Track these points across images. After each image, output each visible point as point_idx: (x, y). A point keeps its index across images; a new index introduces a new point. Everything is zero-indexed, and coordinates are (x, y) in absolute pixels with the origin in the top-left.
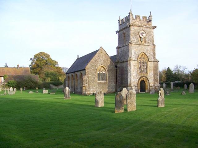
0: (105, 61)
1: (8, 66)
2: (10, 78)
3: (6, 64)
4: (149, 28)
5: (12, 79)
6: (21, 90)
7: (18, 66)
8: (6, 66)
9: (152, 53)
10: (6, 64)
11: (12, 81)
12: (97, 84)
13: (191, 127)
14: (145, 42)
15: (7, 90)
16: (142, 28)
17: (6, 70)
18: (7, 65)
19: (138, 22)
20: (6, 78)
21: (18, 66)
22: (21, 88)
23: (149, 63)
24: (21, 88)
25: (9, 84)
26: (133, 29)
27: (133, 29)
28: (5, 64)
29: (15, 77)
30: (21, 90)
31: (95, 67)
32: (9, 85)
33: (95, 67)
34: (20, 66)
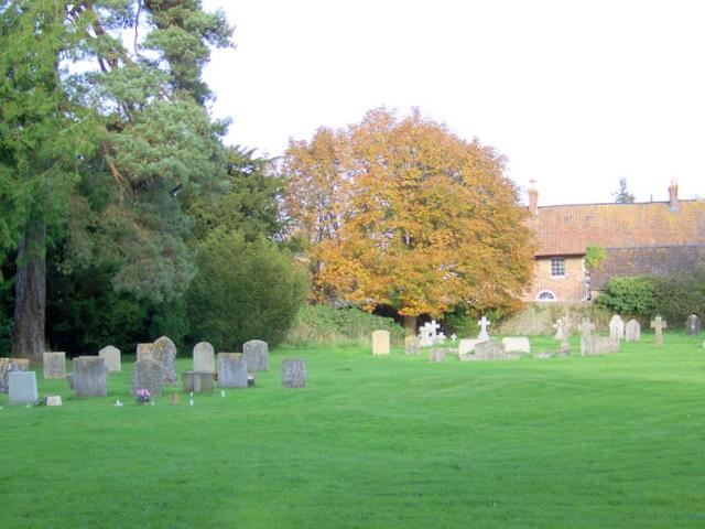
1: (632, 198)
2: (620, 262)
3: (623, 183)
4: (651, 503)
5: (629, 271)
6: (484, 328)
7: (673, 191)
8: (625, 199)
10: (623, 183)
11: (623, 282)
12: (140, 408)
13: (505, 183)
15: (580, 328)
17: (605, 220)
18: (629, 190)
20: (595, 263)
21: (673, 191)
22: (659, 318)
24: (659, 318)
25: (613, 295)
28: (618, 188)
29: (646, 257)
30: (484, 328)
32: (611, 303)
34: (682, 195)
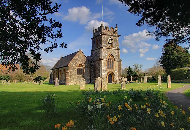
0: (82, 60)
9: (117, 55)
14: (112, 46)
16: (110, 36)
19: (107, 31)
23: (115, 62)
26: (104, 37)
27: (104, 37)
31: (75, 64)
33: (75, 64)
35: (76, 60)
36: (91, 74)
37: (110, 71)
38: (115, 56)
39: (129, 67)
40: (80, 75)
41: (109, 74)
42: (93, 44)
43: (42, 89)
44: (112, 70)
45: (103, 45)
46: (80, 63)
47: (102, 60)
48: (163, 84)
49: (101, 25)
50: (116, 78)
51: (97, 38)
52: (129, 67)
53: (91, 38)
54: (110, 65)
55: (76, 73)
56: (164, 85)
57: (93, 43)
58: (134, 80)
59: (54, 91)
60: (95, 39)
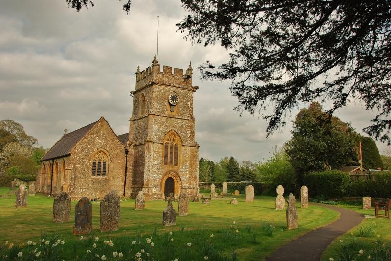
9: (188, 132)
16: (173, 89)
19: (168, 77)
27: (157, 90)
35: (91, 141)
36: (126, 175)
37: (171, 169)
38: (184, 133)
39: (232, 158)
40: (98, 177)
41: (166, 177)
42: (134, 105)
43: (333, 204)
44: (175, 168)
45: (157, 109)
46: (100, 150)
47: (150, 144)
48: (255, 200)
49: (153, 62)
50: (183, 186)
51: (144, 92)
52: (232, 158)
53: (131, 93)
54: (170, 155)
55: (90, 172)
56: (265, 202)
57: (136, 102)
58: (231, 189)
59: (348, 206)
60: (140, 93)
